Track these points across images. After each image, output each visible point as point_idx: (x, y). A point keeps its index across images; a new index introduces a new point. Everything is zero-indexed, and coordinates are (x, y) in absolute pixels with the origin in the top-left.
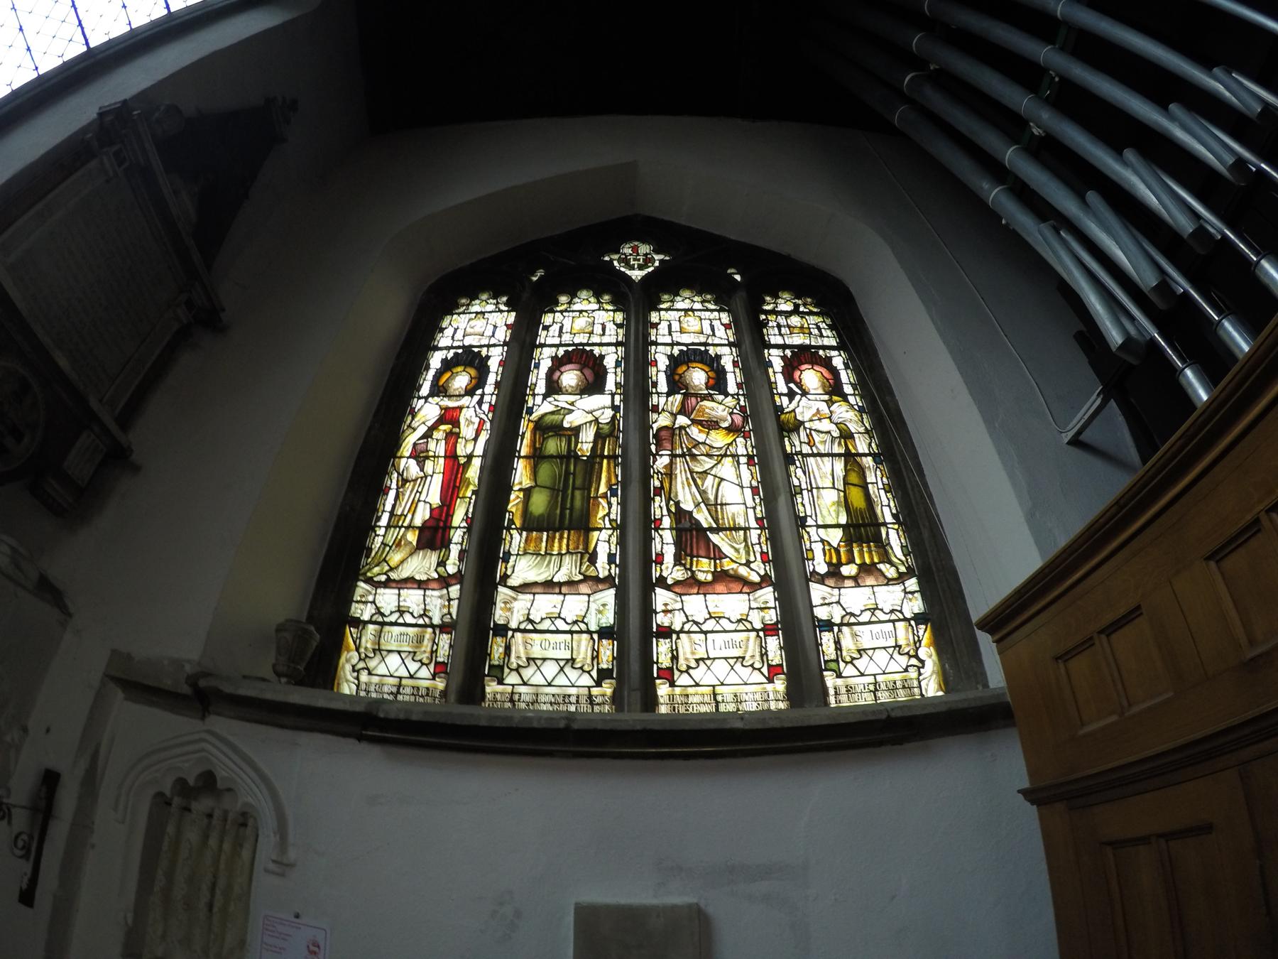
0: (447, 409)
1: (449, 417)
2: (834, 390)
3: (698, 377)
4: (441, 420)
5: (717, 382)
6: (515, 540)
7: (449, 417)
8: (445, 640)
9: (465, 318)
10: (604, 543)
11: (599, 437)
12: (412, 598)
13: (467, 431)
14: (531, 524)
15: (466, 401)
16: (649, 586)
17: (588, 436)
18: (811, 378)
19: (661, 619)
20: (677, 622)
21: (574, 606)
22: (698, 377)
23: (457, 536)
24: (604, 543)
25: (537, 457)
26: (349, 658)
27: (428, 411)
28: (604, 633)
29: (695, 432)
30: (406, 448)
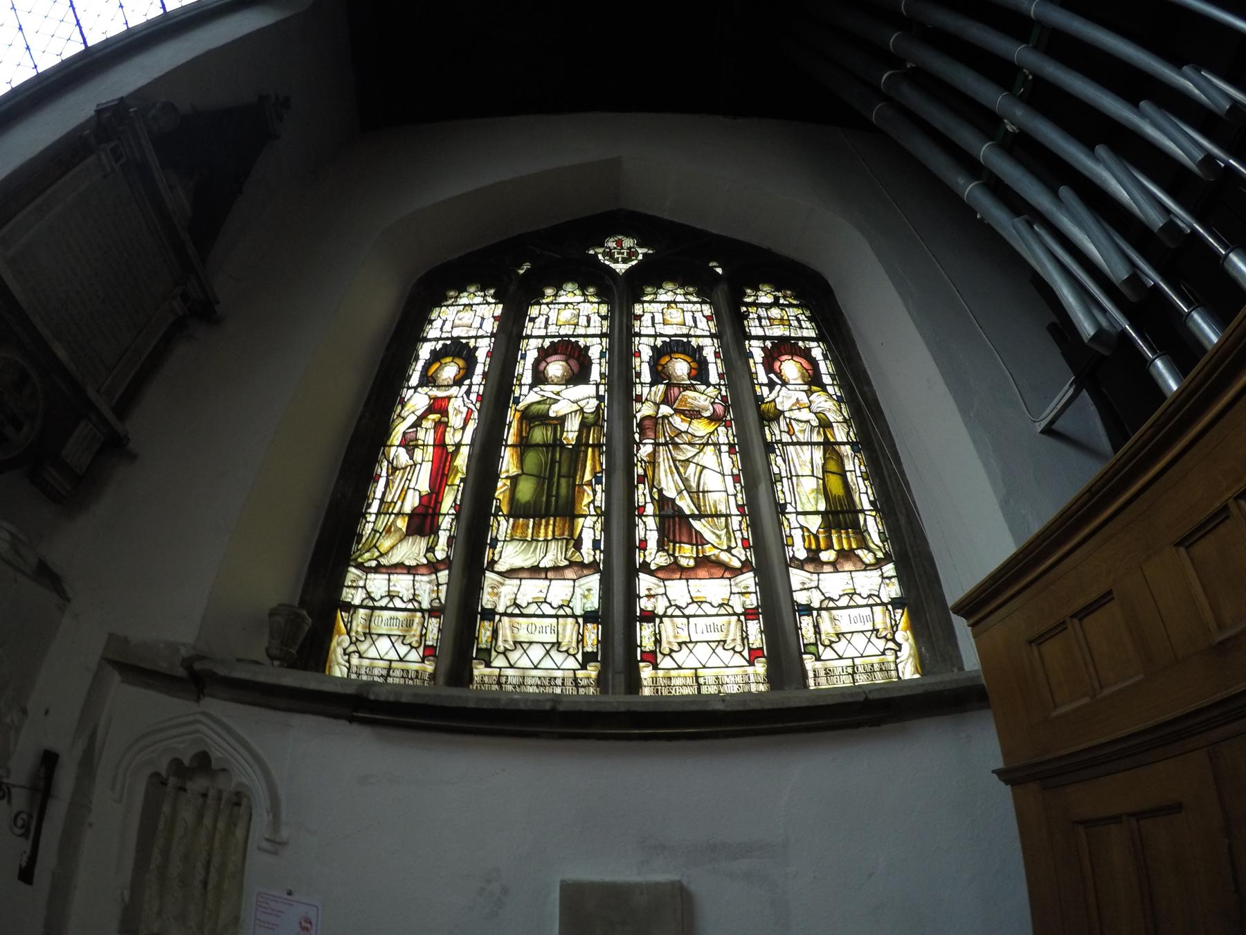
0: (435, 399)
1: (438, 407)
2: (813, 380)
3: (680, 368)
4: (430, 410)
5: (699, 372)
6: (502, 527)
7: (438, 407)
8: (434, 624)
9: (453, 310)
10: (589, 529)
11: (584, 426)
12: (402, 583)
13: (455, 420)
14: (518, 511)
15: (454, 391)
16: (632, 571)
17: (573, 425)
18: (791, 368)
19: (645, 604)
20: (660, 606)
21: (559, 591)
22: (680, 368)
23: (445, 523)
24: (589, 529)
25: (524, 445)
26: (340, 642)
27: (417, 401)
28: (589, 617)
29: (678, 421)
30: (396, 437)
